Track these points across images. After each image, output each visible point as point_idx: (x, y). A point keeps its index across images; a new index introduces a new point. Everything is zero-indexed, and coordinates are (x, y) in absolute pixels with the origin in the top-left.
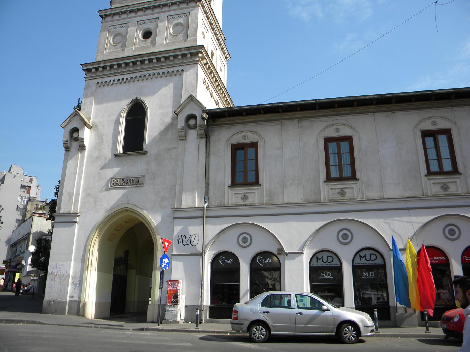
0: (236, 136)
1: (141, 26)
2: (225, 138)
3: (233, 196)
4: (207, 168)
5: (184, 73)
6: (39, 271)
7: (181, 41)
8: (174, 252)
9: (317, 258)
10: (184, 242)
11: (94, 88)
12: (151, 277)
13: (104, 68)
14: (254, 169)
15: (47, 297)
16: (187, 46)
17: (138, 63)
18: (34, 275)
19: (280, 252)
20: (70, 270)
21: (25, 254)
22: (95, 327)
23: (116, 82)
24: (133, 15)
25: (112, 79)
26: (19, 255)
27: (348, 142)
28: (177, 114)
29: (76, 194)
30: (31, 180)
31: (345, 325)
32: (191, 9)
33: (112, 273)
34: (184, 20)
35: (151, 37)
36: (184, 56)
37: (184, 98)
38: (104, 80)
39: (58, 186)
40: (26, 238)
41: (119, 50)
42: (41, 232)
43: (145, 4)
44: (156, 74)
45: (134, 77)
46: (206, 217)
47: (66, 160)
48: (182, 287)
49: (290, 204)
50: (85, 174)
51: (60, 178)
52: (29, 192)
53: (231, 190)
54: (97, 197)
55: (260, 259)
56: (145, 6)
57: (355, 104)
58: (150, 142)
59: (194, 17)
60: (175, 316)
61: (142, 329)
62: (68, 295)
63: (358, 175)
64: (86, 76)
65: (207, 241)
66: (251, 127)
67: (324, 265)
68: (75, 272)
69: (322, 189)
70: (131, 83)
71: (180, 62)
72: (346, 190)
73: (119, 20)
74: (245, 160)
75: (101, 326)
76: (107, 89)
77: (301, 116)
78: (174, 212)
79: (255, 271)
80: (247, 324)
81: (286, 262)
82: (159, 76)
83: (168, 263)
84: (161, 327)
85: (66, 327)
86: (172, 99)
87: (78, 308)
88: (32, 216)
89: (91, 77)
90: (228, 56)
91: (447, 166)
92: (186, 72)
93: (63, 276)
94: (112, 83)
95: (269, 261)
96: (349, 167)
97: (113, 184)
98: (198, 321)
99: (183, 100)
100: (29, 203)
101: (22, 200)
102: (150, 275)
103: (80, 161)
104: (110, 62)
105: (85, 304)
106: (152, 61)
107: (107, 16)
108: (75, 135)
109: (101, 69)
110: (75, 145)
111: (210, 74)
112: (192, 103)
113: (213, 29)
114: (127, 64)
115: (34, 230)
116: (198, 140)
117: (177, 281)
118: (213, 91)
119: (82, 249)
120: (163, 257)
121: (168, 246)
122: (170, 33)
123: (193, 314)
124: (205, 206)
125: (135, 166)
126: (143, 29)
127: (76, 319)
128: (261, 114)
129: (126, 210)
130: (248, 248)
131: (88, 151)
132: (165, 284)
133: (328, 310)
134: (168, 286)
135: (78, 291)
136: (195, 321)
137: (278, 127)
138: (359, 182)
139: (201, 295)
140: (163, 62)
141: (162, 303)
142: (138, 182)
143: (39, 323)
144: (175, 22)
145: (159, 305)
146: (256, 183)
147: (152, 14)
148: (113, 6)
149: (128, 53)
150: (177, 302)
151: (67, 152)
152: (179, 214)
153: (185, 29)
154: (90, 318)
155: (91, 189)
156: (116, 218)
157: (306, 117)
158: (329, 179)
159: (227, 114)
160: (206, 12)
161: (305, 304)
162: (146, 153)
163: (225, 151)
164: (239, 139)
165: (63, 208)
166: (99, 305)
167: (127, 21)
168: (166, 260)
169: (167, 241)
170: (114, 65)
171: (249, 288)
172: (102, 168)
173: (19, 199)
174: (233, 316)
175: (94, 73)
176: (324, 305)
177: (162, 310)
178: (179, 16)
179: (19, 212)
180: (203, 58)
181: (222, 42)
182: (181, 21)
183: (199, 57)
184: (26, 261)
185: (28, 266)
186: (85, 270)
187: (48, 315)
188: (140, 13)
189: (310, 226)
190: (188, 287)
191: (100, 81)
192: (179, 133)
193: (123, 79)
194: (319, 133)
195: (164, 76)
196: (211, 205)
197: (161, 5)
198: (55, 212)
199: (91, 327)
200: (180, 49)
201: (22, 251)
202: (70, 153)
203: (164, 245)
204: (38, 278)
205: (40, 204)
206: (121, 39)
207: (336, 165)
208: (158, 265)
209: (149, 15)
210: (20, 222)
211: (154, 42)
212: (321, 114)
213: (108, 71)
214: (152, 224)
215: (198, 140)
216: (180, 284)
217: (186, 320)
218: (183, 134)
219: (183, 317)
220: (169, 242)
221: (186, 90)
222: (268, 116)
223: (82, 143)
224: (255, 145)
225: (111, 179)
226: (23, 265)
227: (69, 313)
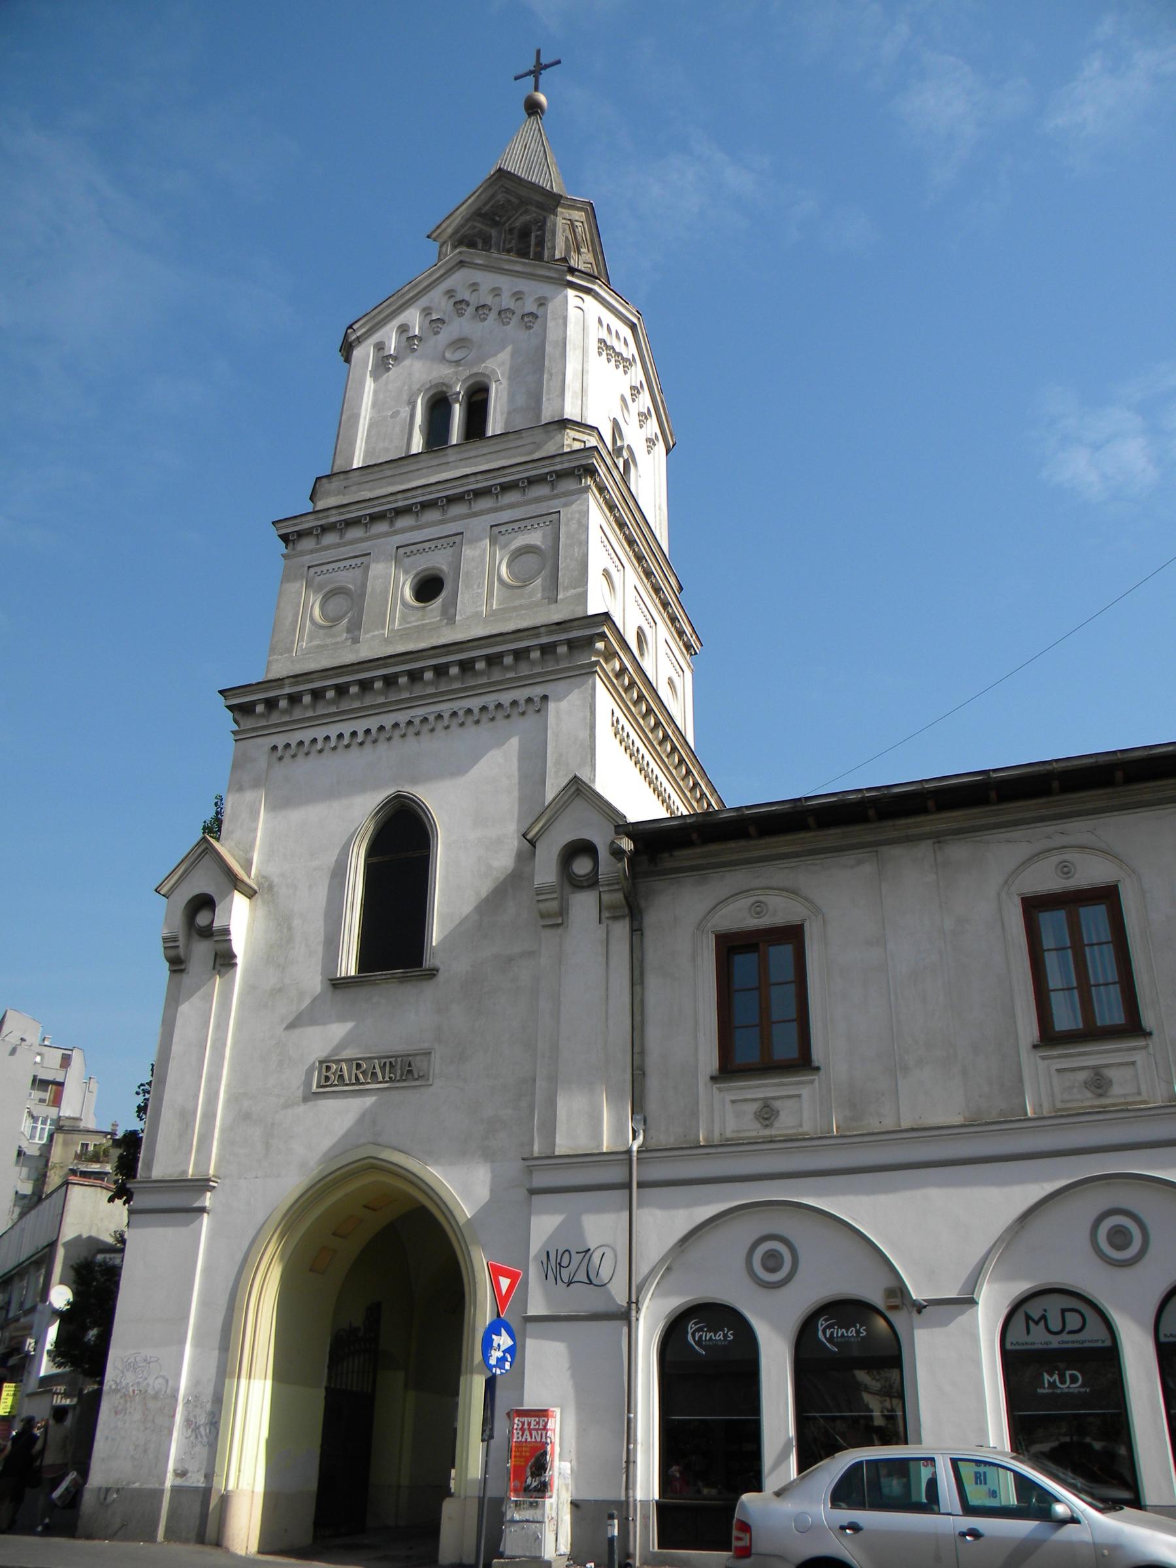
0: (731, 907)
2: (693, 915)
3: (728, 1111)
4: (638, 1018)
5: (552, 706)
6: (81, 1377)
8: (531, 1312)
9: (1028, 1317)
10: (565, 1274)
12: (456, 1393)
13: (294, 699)
14: (794, 1016)
16: (556, 617)
17: (403, 680)
20: (179, 1375)
21: (36, 1318)
24: (382, 527)
25: (320, 733)
26: (17, 1319)
28: (533, 843)
30: (66, 1061)
32: (563, 500)
33: (324, 1383)
34: (544, 536)
35: (443, 594)
36: (547, 650)
38: (294, 738)
39: (150, 1084)
40: (42, 1259)
41: (339, 639)
42: (91, 1239)
43: (419, 491)
44: (461, 713)
46: (640, 1185)
47: (173, 1000)
48: (561, 1434)
49: (921, 1132)
50: (232, 1049)
51: (153, 1059)
52: (57, 1101)
53: (720, 1090)
55: (829, 1327)
56: (421, 499)
58: (445, 938)
59: (574, 526)
60: (538, 1540)
63: (1148, 1019)
64: (235, 727)
65: (642, 1268)
66: (777, 874)
67: (1055, 1342)
68: (195, 1382)
70: (382, 747)
72: (1111, 1073)
73: (339, 545)
74: (763, 986)
76: (303, 767)
78: (530, 1170)
79: (810, 1366)
82: (470, 719)
83: (511, 1350)
86: (516, 794)
87: (203, 1517)
88: (66, 1183)
89: (254, 729)
90: (693, 640)
92: (559, 699)
93: (155, 1397)
94: (319, 746)
95: (858, 1332)
96: (1115, 992)
97: (327, 1078)
100: (59, 1138)
103: (219, 1002)
105: (225, 1499)
106: (447, 673)
107: (301, 535)
108: (202, 919)
109: (283, 704)
110: (202, 950)
111: (636, 703)
112: (579, 805)
113: (640, 558)
114: (366, 686)
115: (69, 1233)
116: (604, 926)
117: (543, 1414)
118: (648, 757)
120: (495, 1327)
121: (511, 1287)
124: (635, 1148)
125: (402, 1017)
128: (805, 828)
129: (374, 1166)
130: (784, 1290)
131: (246, 971)
133: (1074, 1520)
134: (511, 1432)
137: (868, 869)
138: (1153, 1043)
139: (628, 1462)
140: (482, 673)
141: (489, 1494)
142: (410, 1072)
144: (515, 545)
145: (481, 1500)
146: (802, 1062)
147: (442, 522)
148: (321, 505)
150: (543, 1489)
151: (177, 975)
152: (549, 1176)
153: (553, 565)
155: (253, 1099)
156: (340, 1194)
158: (1049, 1037)
159: (694, 836)
160: (612, 507)
161: (993, 1494)
162: (432, 973)
163: (694, 959)
164: (738, 916)
165: (160, 1163)
167: (363, 547)
168: (503, 1341)
169: (507, 1274)
170: (325, 689)
171: (792, 1432)
172: (291, 1026)
173: (26, 1125)
175: (262, 715)
177: (492, 1518)
179: (25, 1170)
180: (610, 655)
181: (671, 598)
182: (535, 538)
183: (598, 653)
184: (40, 1341)
185: (45, 1358)
186: (232, 1377)
188: (403, 522)
189: (1000, 1201)
191: (280, 740)
192: (542, 906)
194: (1006, 882)
196: (652, 1144)
197: (468, 492)
198: (135, 1177)
200: (533, 631)
201: (28, 1305)
202: (186, 979)
203: (496, 1286)
204: (75, 1401)
205: (92, 1142)
206: (349, 607)
208: (478, 1356)
209: (432, 526)
210: (26, 1201)
213: (306, 707)
214: (457, 1213)
215: (604, 926)
216: (554, 1424)
218: (554, 905)
219: (565, 1547)
221: (557, 763)
222: (833, 836)
223: (225, 945)
224: (793, 935)
225: (321, 1062)
226: (27, 1354)
227: (171, 1534)
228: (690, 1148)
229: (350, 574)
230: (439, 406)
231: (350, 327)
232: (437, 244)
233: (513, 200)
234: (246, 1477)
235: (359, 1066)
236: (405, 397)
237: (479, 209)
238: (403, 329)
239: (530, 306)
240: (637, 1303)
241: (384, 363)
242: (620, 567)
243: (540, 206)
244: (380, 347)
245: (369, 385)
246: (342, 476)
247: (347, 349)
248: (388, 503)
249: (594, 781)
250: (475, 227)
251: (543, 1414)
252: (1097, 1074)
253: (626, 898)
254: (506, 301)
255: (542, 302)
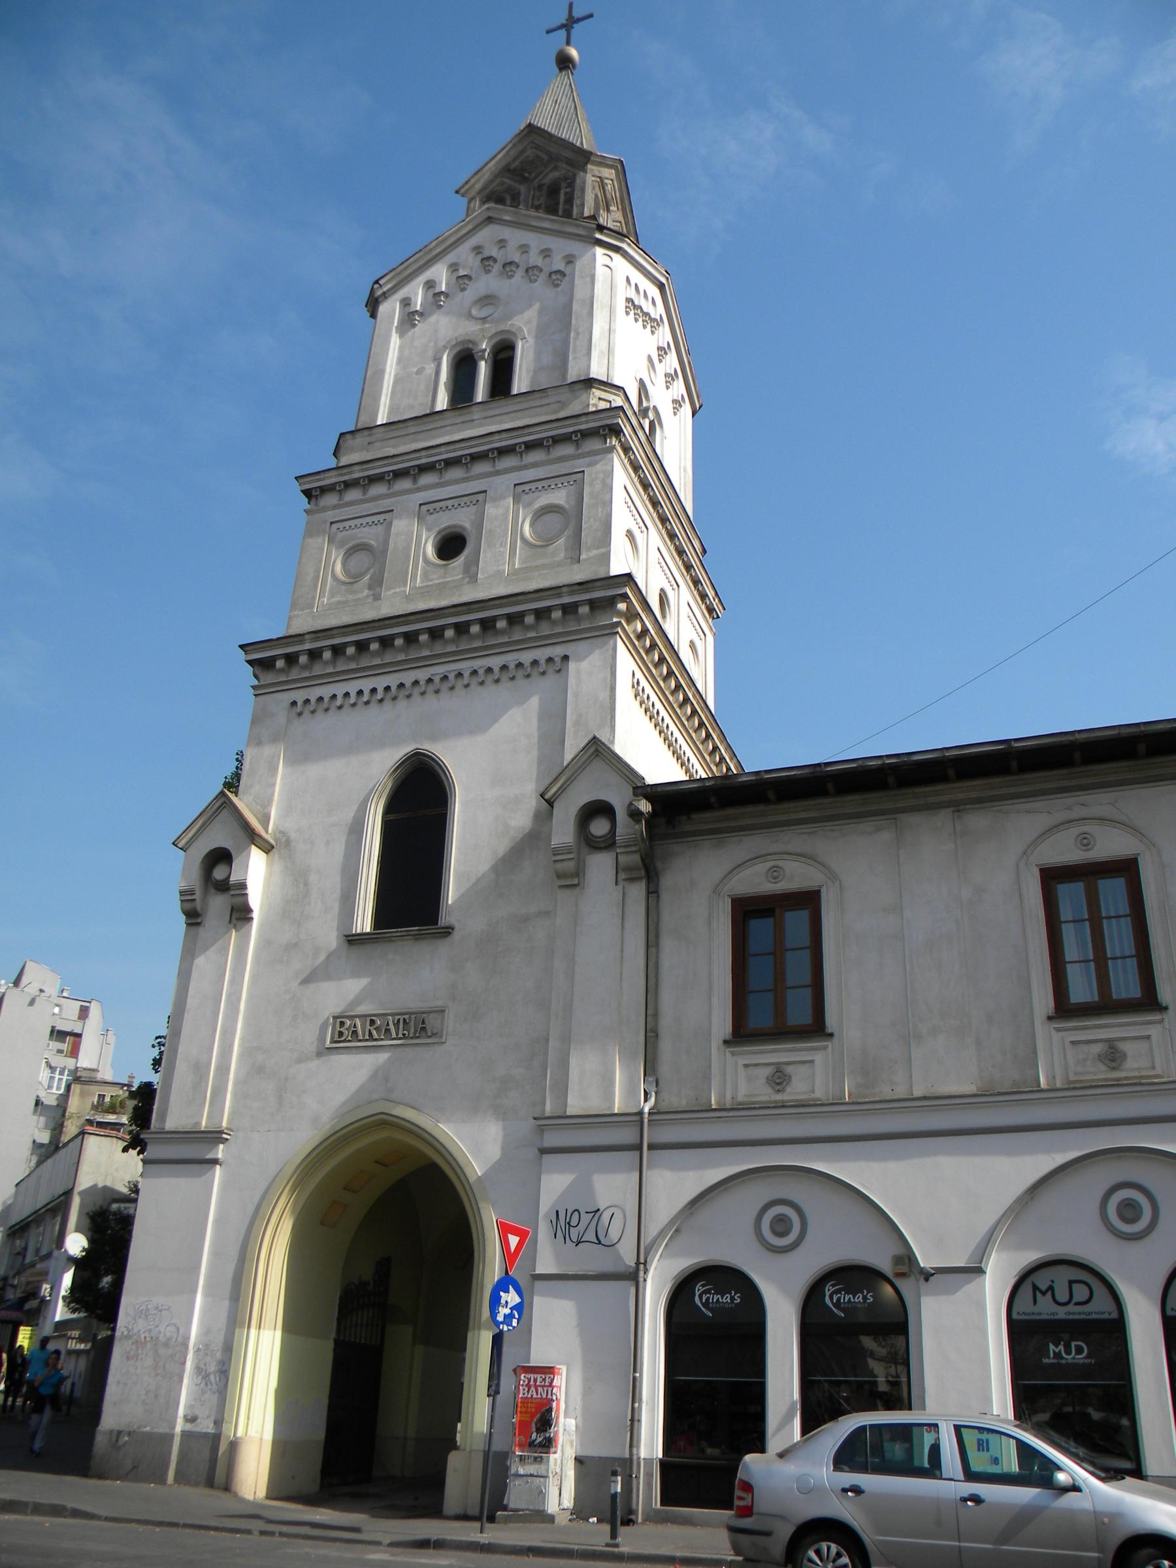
0: (748, 872)
1: (430, 518)
2: (710, 878)
3: (739, 1076)
4: (652, 981)
5: (572, 666)
6: (95, 1322)
7: (559, 564)
8: (539, 1270)
9: (1035, 1288)
10: (574, 1233)
11: (282, 719)
12: (463, 1349)
13: (315, 655)
15: (110, 1419)
16: (579, 578)
18: (76, 1333)
19: (904, 1269)
20: (190, 1323)
21: (52, 1264)
22: (262, 1533)
23: (352, 700)
24: (405, 484)
25: (339, 689)
26: (33, 1265)
27: (1122, 881)
28: (550, 803)
29: (218, 1068)
30: (84, 1013)
31: (1145, 1552)
32: (587, 460)
33: (333, 1335)
34: (568, 496)
36: (569, 610)
37: (572, 747)
38: (313, 694)
40: (58, 1207)
41: (360, 596)
42: (106, 1189)
43: (443, 449)
44: (481, 672)
45: (408, 684)
48: (567, 1392)
52: (74, 1052)
53: (733, 1054)
54: (286, 1079)
55: (836, 1292)
56: (444, 457)
57: (1142, 748)
59: (598, 486)
60: (541, 1494)
61: (423, 1544)
62: (181, 1412)
64: (256, 682)
65: (652, 1229)
66: (793, 840)
67: (1061, 1313)
68: (206, 1331)
69: (1040, 1045)
70: (402, 704)
71: (559, 630)
72: (1125, 1047)
74: (778, 952)
75: (285, 1529)
76: (324, 723)
77: (961, 796)
78: (541, 1129)
80: (785, 1532)
81: (922, 1299)
82: (490, 679)
84: (492, 1534)
85: (166, 1529)
87: (212, 1460)
88: (83, 1133)
91: (1125, 984)
92: (580, 659)
93: (166, 1344)
94: (339, 702)
95: (865, 1298)
97: (341, 1034)
98: (619, 1514)
99: (568, 756)
100: (76, 1089)
101: (52, 1078)
102: (454, 1342)
104: (332, 637)
105: (234, 1446)
106: (468, 631)
107: (324, 490)
108: (219, 873)
109: (303, 659)
110: (218, 904)
112: (598, 766)
115: (85, 1181)
116: (620, 887)
117: (549, 1371)
118: (668, 720)
119: (234, 1252)
120: (505, 1283)
121: (520, 1245)
122: (523, 539)
123: (605, 1489)
124: (646, 1110)
125: (416, 975)
126: (437, 529)
127: (200, 1501)
129: (384, 1122)
131: (262, 926)
132: (507, 1381)
133: (1075, 1488)
134: (517, 1388)
135: (214, 1399)
136: (609, 1515)
137: (886, 836)
138: (1168, 1017)
139: (632, 1420)
140: (503, 632)
141: (494, 1448)
142: (423, 1029)
143: (76, 1513)
144: (538, 504)
145: (486, 1454)
146: (816, 1028)
148: (344, 461)
149: (393, 602)
150: (548, 1444)
151: (193, 928)
152: (559, 1135)
153: (577, 524)
154: (249, 1496)
157: (980, 800)
158: (1064, 1009)
159: (713, 799)
160: (636, 468)
161: (996, 1461)
162: (448, 931)
164: (755, 881)
165: (174, 1115)
166: (282, 1449)
171: (796, 1395)
172: (306, 981)
173: (44, 1075)
174: (737, 1503)
175: (282, 671)
176: (1059, 1469)
177: (496, 1470)
178: (552, 482)
179: (42, 1119)
180: (632, 616)
182: (559, 497)
183: (619, 614)
184: (55, 1287)
187: (108, 1482)
188: (427, 479)
190: (587, 1390)
191: (299, 696)
192: (559, 866)
193: (374, 691)
195: (505, 677)
196: (664, 1106)
198: (149, 1128)
199: (249, 1532)
200: (555, 590)
201: (44, 1252)
202: (202, 931)
203: (505, 1243)
204: (89, 1346)
205: (109, 1093)
206: (368, 561)
207: (1088, 961)
209: (455, 484)
210: (43, 1150)
211: (474, 569)
212: (1026, 789)
213: (326, 663)
215: (620, 887)
216: (560, 1381)
217: (580, 1512)
218: (570, 866)
219: (568, 1501)
220: (522, 1234)
221: (577, 723)
224: (809, 900)
225: (335, 1018)
227: (181, 1478)
228: (701, 1111)
229: (373, 530)
230: (464, 363)
231: (377, 282)
232: (465, 200)
233: (545, 157)
234: (256, 1423)
235: (372, 1022)
236: (430, 353)
237: (509, 164)
238: (430, 284)
239: (559, 265)
240: (645, 1264)
241: (410, 319)
242: (644, 528)
243: (570, 163)
244: (406, 302)
245: (395, 341)
246: (366, 433)
247: (373, 304)
248: (411, 460)
249: (613, 742)
250: (503, 183)
251: (549, 1371)
252: (1111, 1047)
253: (643, 859)
254: (535, 259)
255: (570, 260)
